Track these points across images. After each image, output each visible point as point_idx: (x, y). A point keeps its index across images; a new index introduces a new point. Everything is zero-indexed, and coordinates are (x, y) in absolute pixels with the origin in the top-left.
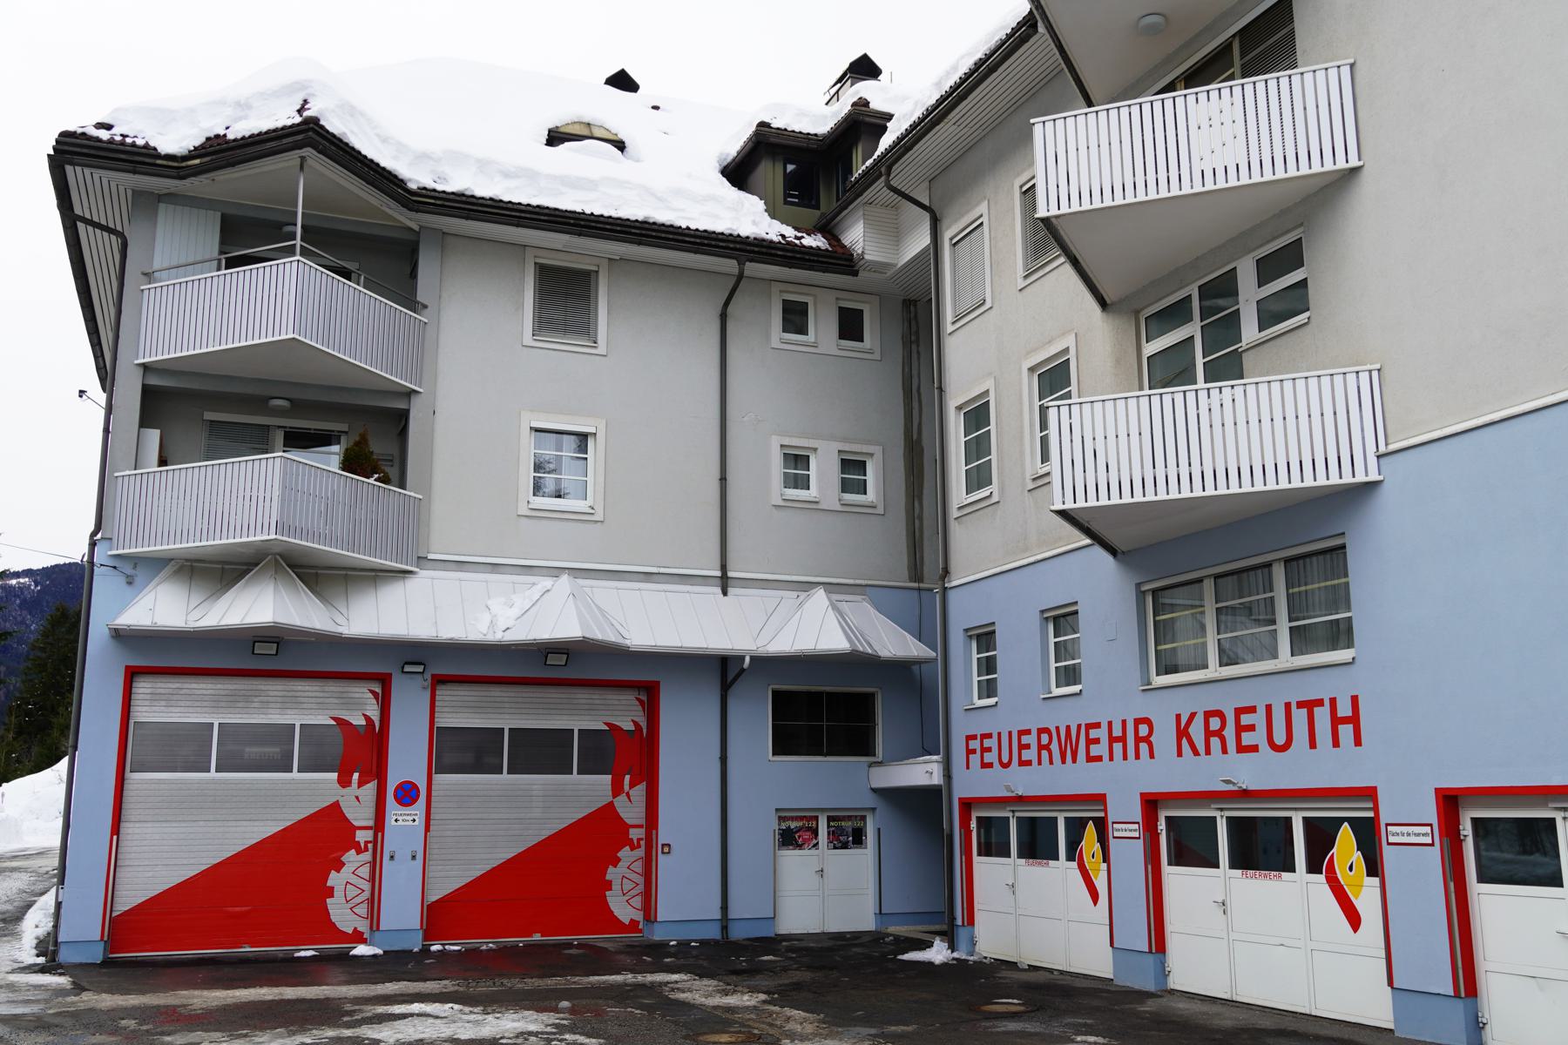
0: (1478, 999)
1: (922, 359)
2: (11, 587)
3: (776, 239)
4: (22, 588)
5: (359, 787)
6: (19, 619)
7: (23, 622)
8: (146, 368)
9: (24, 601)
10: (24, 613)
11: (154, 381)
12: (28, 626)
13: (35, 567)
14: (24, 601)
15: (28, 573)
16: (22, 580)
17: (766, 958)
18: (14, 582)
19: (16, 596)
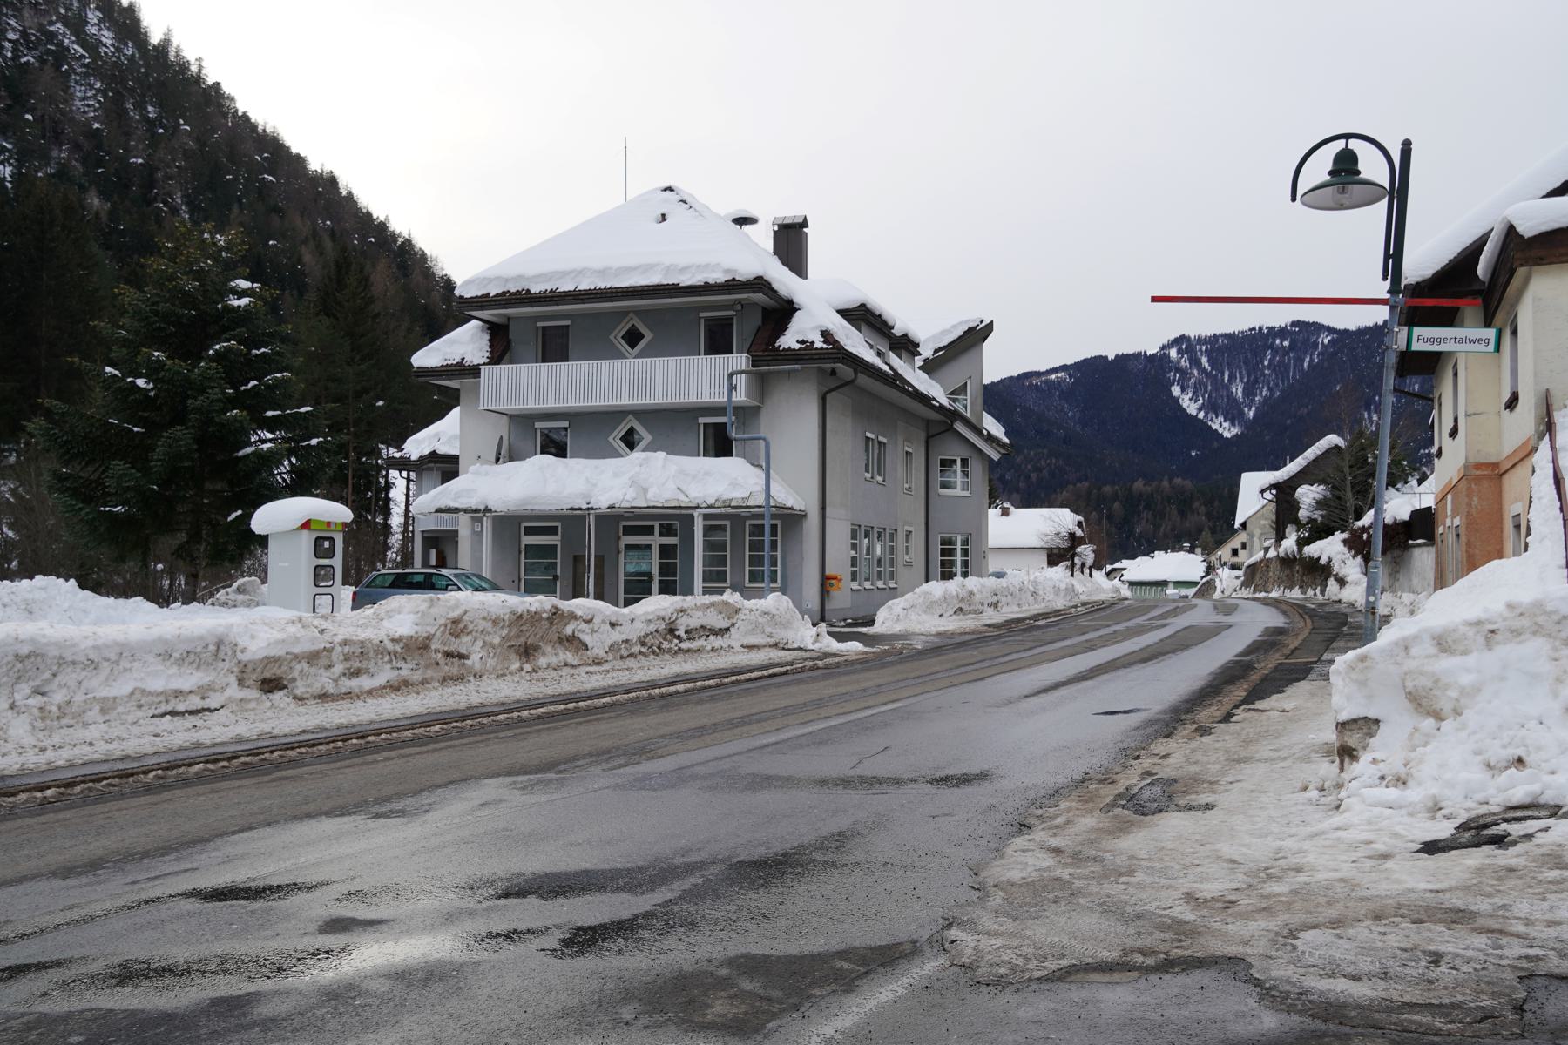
0: (312, 518)
1: (181, 954)
2: (1052, 381)
3: (797, 346)
4: (1061, 381)
5: (354, 608)
6: (1059, 408)
7: (1062, 410)
8: (423, 532)
9: (1062, 392)
10: (1063, 402)
11: (425, 535)
12: (1066, 414)
13: (1069, 363)
14: (1062, 392)
15: (1064, 368)
16: (1059, 375)
17: (233, 516)
18: (1053, 377)
19: (1056, 389)
